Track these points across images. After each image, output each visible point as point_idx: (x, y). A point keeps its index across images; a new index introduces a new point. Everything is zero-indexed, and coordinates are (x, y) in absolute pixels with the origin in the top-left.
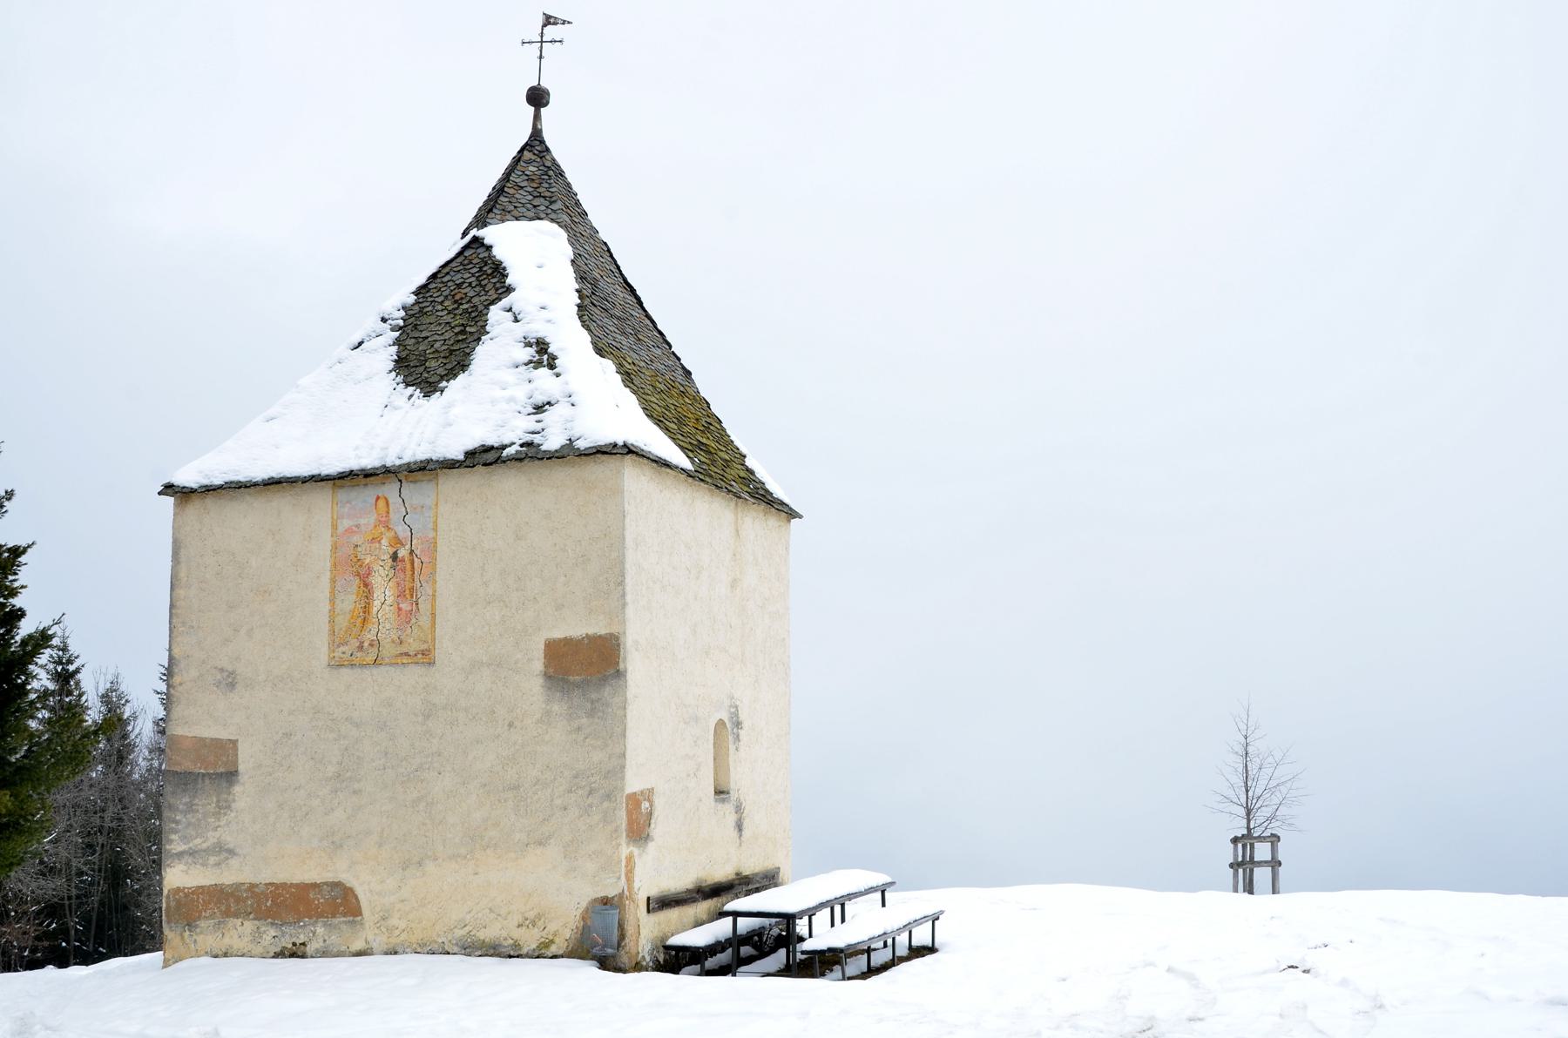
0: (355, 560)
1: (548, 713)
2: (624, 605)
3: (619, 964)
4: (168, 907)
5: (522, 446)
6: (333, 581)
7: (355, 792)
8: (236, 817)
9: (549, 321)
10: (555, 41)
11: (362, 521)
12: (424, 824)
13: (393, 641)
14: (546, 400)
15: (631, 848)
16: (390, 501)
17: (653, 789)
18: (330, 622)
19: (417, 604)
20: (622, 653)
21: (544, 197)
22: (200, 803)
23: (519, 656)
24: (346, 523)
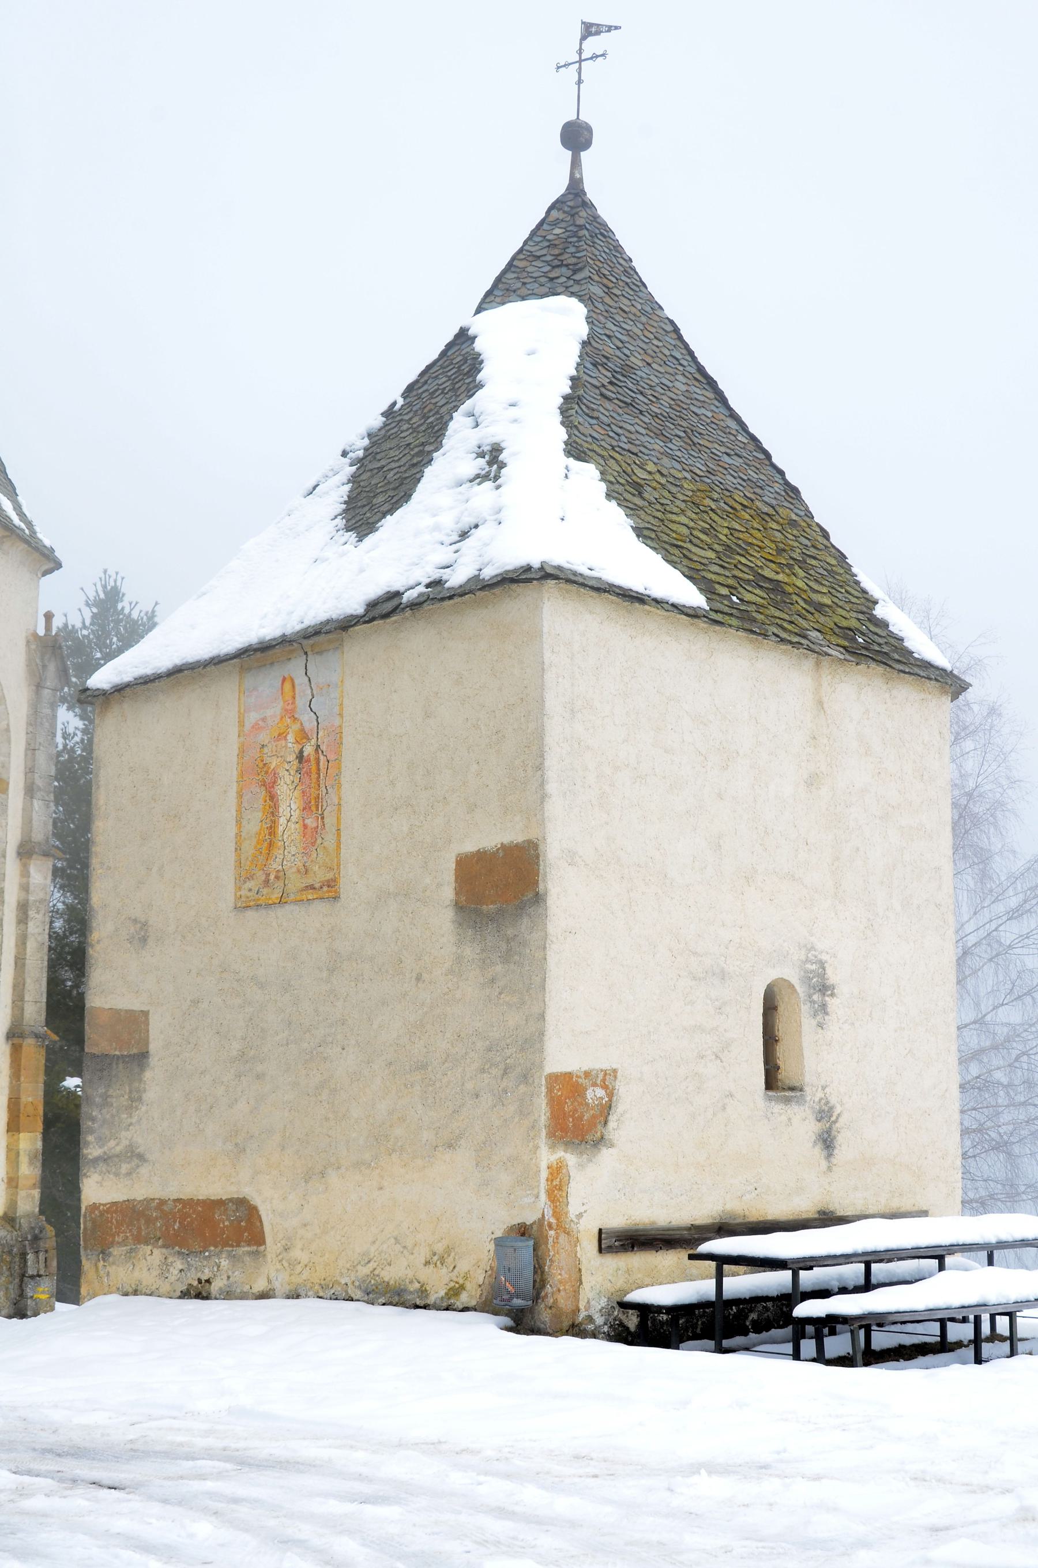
0: (261, 765)
1: (459, 959)
2: (543, 798)
3: (538, 1323)
4: (85, 1229)
5: (428, 586)
6: (240, 795)
7: (258, 1077)
8: (147, 1112)
9: (515, 421)
10: (597, 56)
11: (269, 713)
12: (327, 1119)
13: (299, 871)
14: (473, 521)
15: (560, 1154)
16: (297, 682)
17: (615, 1071)
18: (236, 849)
19: (323, 818)
20: (541, 868)
21: (567, 265)
22: (114, 1094)
23: (428, 881)
24: (253, 717)
